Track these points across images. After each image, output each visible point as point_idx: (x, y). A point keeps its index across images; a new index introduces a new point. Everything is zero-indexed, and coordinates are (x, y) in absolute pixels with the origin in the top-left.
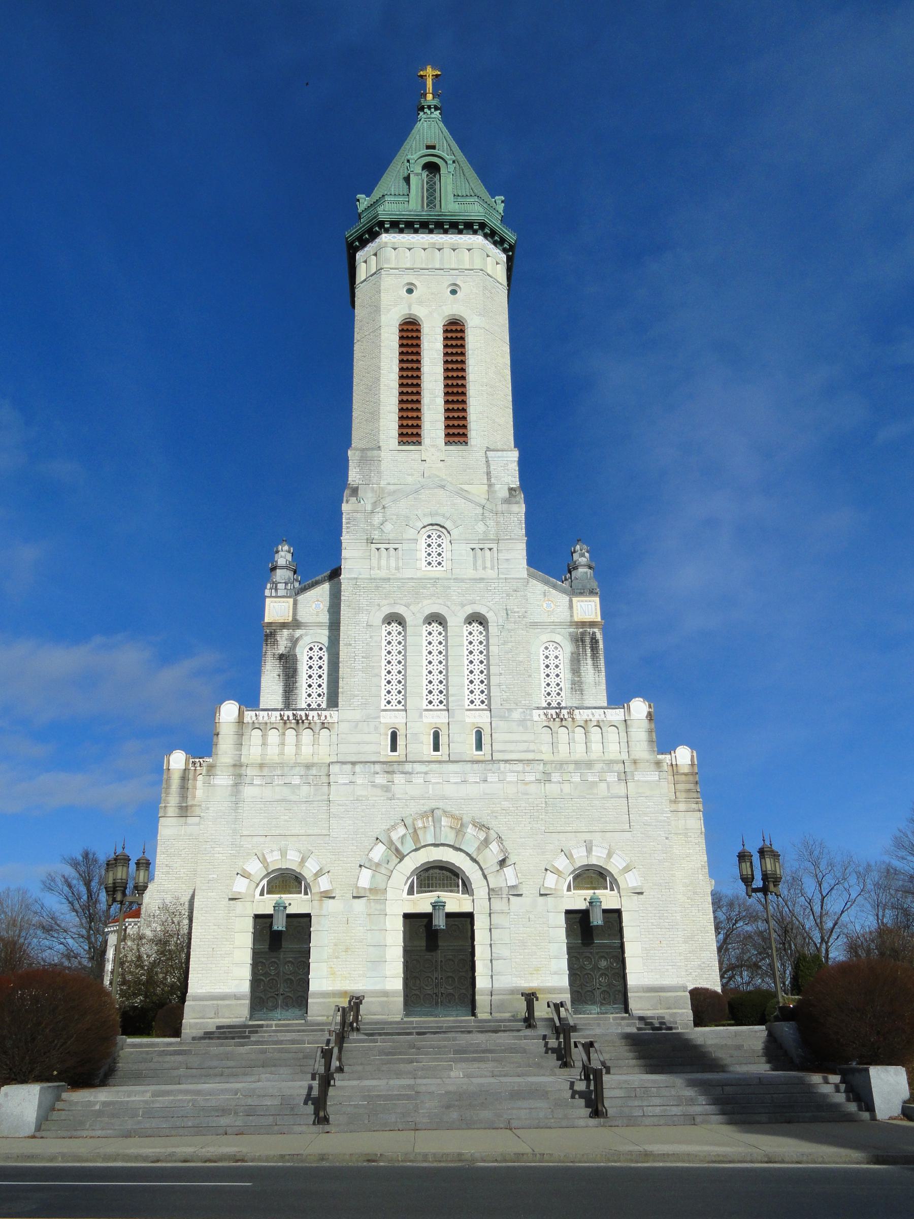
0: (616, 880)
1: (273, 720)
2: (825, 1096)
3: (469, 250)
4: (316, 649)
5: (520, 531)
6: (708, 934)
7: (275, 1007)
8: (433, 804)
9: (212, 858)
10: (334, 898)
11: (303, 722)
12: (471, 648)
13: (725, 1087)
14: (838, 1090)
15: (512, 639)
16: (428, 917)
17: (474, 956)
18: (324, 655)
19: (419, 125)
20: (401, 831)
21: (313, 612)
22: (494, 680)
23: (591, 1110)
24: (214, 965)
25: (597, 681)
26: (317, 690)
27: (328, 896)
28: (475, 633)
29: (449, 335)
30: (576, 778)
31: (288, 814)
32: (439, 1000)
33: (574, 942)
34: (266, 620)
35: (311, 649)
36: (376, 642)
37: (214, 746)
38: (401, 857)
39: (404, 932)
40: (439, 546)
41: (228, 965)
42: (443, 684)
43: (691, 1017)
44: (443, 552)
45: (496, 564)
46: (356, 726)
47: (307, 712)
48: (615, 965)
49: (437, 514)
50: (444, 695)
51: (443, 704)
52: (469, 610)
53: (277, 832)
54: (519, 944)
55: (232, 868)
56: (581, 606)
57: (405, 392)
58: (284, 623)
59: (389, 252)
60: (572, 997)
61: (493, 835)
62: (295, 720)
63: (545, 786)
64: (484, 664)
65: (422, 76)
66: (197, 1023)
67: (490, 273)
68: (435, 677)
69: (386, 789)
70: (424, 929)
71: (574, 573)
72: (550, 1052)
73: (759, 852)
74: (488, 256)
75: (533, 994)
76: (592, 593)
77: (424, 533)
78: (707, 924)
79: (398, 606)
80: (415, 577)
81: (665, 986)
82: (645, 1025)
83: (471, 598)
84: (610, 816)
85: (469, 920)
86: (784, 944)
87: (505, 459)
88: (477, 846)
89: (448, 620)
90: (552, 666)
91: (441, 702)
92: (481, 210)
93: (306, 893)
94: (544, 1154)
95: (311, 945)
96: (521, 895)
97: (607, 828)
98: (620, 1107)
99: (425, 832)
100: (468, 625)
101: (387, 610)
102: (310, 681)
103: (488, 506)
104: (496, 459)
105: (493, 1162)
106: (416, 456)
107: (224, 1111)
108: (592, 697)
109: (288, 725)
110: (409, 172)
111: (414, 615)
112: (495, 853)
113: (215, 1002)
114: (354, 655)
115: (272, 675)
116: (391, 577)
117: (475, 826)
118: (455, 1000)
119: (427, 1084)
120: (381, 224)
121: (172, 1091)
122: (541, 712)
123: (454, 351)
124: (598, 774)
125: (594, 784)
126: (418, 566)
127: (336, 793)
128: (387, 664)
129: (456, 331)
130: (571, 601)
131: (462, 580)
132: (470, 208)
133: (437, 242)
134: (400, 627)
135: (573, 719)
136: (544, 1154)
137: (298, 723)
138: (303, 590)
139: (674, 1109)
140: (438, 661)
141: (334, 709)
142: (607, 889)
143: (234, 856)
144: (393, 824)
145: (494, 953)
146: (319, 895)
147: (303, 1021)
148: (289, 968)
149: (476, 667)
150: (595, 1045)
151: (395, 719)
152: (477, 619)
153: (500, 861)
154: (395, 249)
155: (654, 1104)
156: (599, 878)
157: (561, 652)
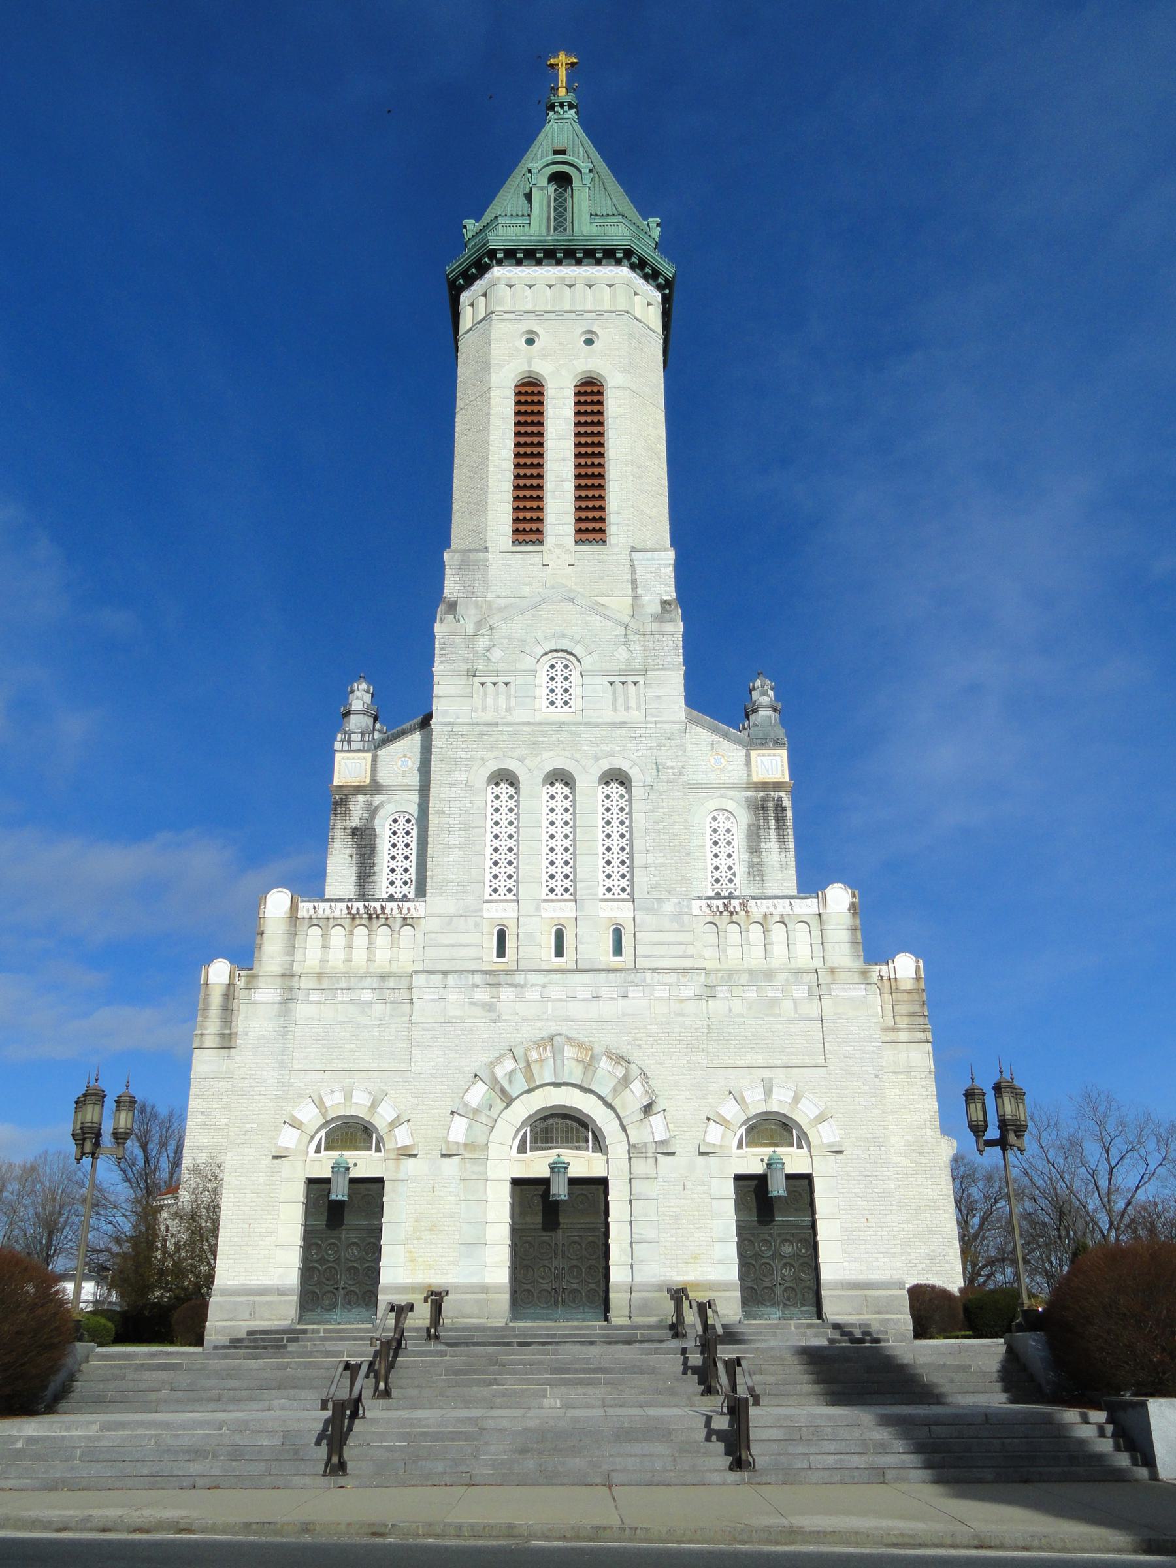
0: (805, 1133)
1: (337, 914)
2: (1082, 1442)
3: (610, 286)
4: (402, 821)
5: (677, 659)
6: (939, 1211)
7: (333, 1307)
8: (553, 1028)
9: (250, 1101)
10: (415, 1156)
11: (378, 917)
12: (608, 816)
13: (933, 1427)
14: (1102, 1433)
15: (664, 804)
16: (545, 1182)
17: (609, 1237)
18: (412, 829)
19: (548, 127)
20: (509, 1064)
21: (399, 771)
22: (638, 859)
23: (731, 1458)
24: (251, 1248)
25: (783, 863)
26: (402, 877)
27: (407, 1153)
28: (614, 797)
29: (583, 399)
30: (751, 993)
31: (355, 1042)
32: (560, 1299)
33: (746, 1219)
34: (336, 783)
35: (395, 821)
36: (478, 808)
37: (256, 950)
38: (509, 1101)
39: (513, 1205)
40: (566, 679)
41: (269, 1248)
42: (569, 866)
43: (910, 1325)
44: (570, 687)
45: (642, 703)
46: (450, 923)
47: (383, 904)
48: (803, 1251)
49: (563, 636)
50: (571, 881)
51: (569, 893)
52: (605, 765)
53: (341, 1066)
54: (670, 1222)
55: (278, 1114)
56: (762, 762)
57: (583, 528)
58: (359, 786)
59: (502, 290)
60: (743, 1297)
61: (634, 1070)
62: (368, 914)
63: (707, 1004)
64: (625, 839)
65: (552, 66)
66: (225, 1327)
67: (639, 317)
68: (559, 856)
69: (489, 1007)
70: (540, 1199)
71: (752, 717)
72: (689, 1372)
73: (994, 1088)
74: (636, 294)
75: (684, 1290)
76: (777, 743)
77: (546, 662)
78: (939, 1197)
79: (509, 760)
80: (532, 721)
81: (873, 1281)
82: (841, 1336)
83: (608, 749)
84: (798, 1046)
85: (601, 1188)
86: (1059, 1230)
87: (657, 562)
88: (612, 1086)
89: (576, 778)
90: (722, 843)
91: (566, 890)
92: (627, 232)
93: (378, 1150)
94: (636, 1529)
95: (383, 1220)
96: (673, 1154)
97: (794, 1061)
98: (776, 1454)
99: (542, 1066)
100: (604, 786)
101: (493, 766)
102: (393, 864)
103: (633, 624)
104: (643, 562)
105: (559, 1539)
106: (536, 559)
107: (197, 1454)
108: (776, 884)
109: (358, 922)
110: (531, 185)
111: (530, 773)
112: (638, 1095)
113: (251, 1298)
114: (448, 826)
115: (342, 856)
116: (500, 721)
117: (611, 1059)
118: (581, 1298)
119: (504, 1417)
120: (492, 254)
121: (129, 1423)
122: (704, 903)
123: (589, 419)
124: (780, 988)
125: (775, 1001)
126: (537, 706)
127: (422, 1014)
128: (493, 839)
129: (592, 393)
130: (748, 755)
131: (597, 725)
132: (611, 230)
133: (566, 276)
134: (512, 789)
135: (747, 912)
136: (636, 1529)
137: (370, 918)
138: (386, 742)
139: (855, 1458)
140: (563, 834)
141: (420, 900)
142: (793, 1146)
143: (279, 1098)
144: (498, 1056)
145: (636, 1234)
146: (396, 1152)
147: (370, 1326)
148: (353, 1252)
149: (615, 843)
150: (743, 1363)
151: (503, 913)
152: (617, 777)
153: (645, 1107)
154: (510, 286)
155: (828, 1451)
156: (781, 1130)
157: (735, 825)
